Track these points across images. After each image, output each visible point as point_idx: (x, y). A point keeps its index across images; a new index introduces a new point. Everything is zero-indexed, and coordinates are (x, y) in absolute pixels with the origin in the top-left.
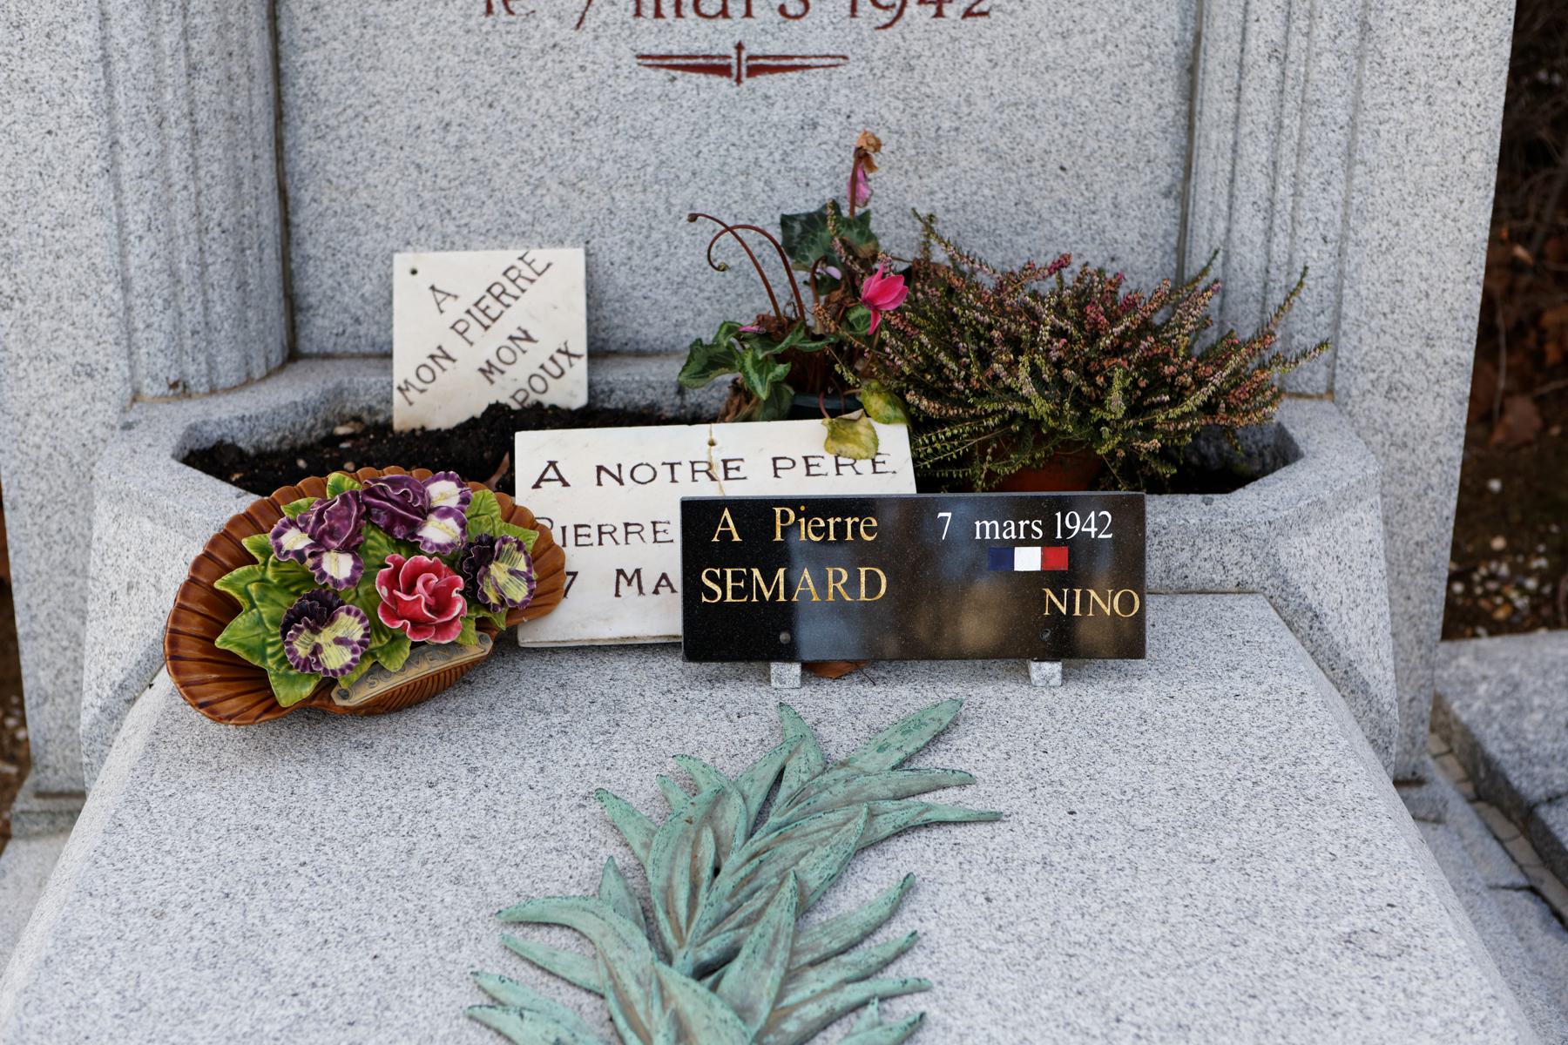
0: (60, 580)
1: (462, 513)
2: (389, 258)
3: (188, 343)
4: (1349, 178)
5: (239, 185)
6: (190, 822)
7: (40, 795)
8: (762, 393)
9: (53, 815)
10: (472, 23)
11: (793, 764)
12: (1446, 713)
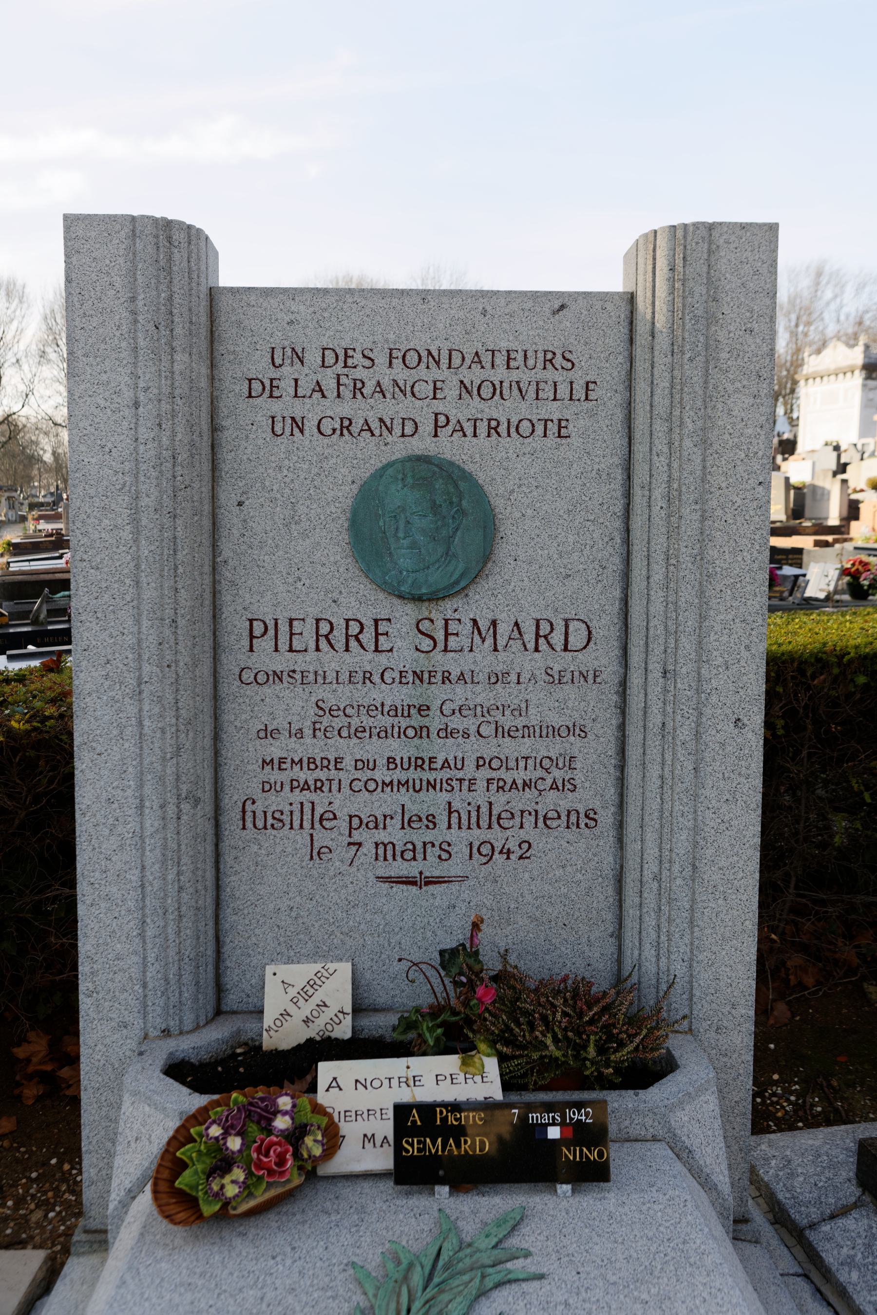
0: (104, 1124)
1: (292, 1113)
2: (263, 968)
3: (171, 1011)
4: (692, 933)
5: (198, 938)
6: (158, 1281)
7: (86, 1232)
8: (431, 1042)
9: (91, 1243)
10: (304, 864)
11: (446, 1245)
12: (757, 1175)
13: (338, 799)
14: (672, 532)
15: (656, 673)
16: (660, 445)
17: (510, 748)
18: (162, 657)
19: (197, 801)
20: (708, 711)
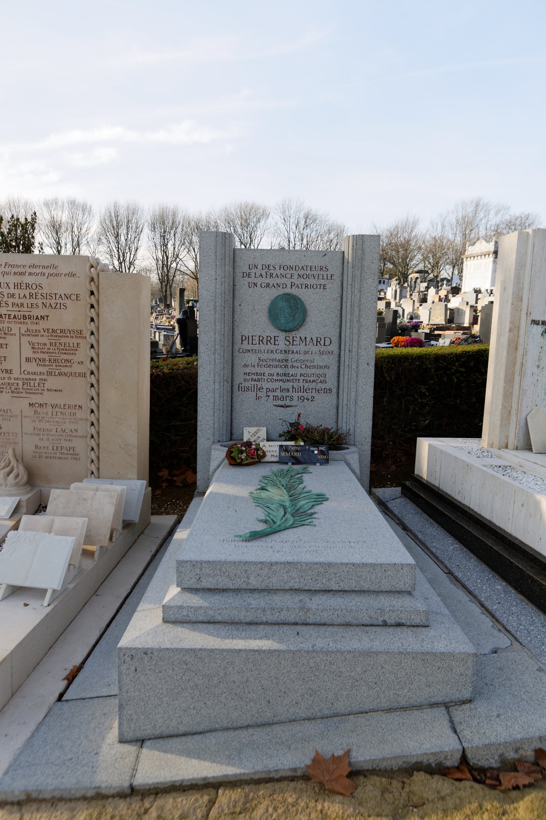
13: (264, 384)
14: (352, 314)
15: (347, 351)
16: (349, 292)
17: (309, 371)
18: (220, 344)
19: (228, 382)
20: (360, 361)
